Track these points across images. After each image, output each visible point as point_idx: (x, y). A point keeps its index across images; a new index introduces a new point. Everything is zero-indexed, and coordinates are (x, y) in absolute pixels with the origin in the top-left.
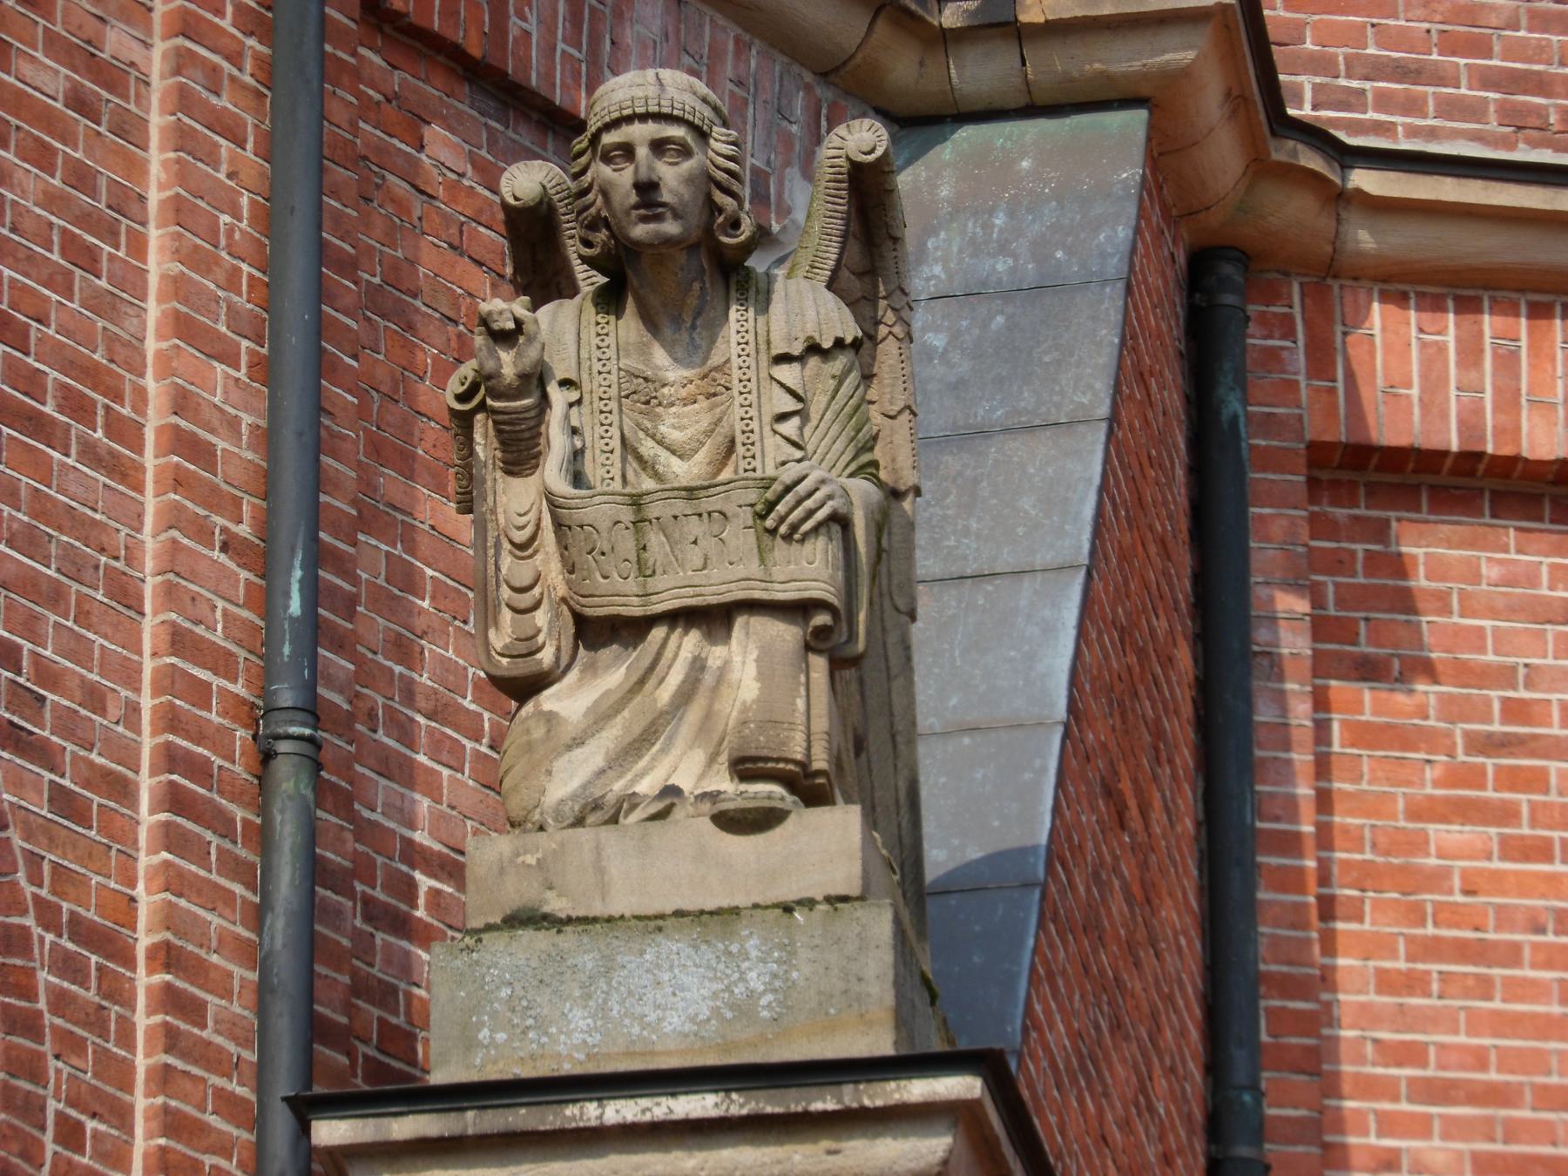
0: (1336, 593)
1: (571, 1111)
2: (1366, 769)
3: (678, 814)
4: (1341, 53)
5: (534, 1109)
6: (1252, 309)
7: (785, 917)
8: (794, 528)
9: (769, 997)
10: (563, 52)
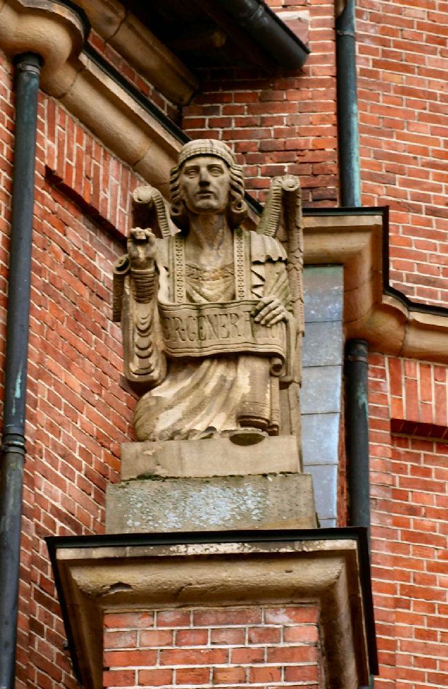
0: (400, 480)
1: (173, 548)
2: (411, 550)
3: (216, 437)
4: (404, 273)
5: (156, 547)
6: (371, 366)
7: (264, 480)
8: (267, 322)
9: (257, 511)
10: (120, 210)
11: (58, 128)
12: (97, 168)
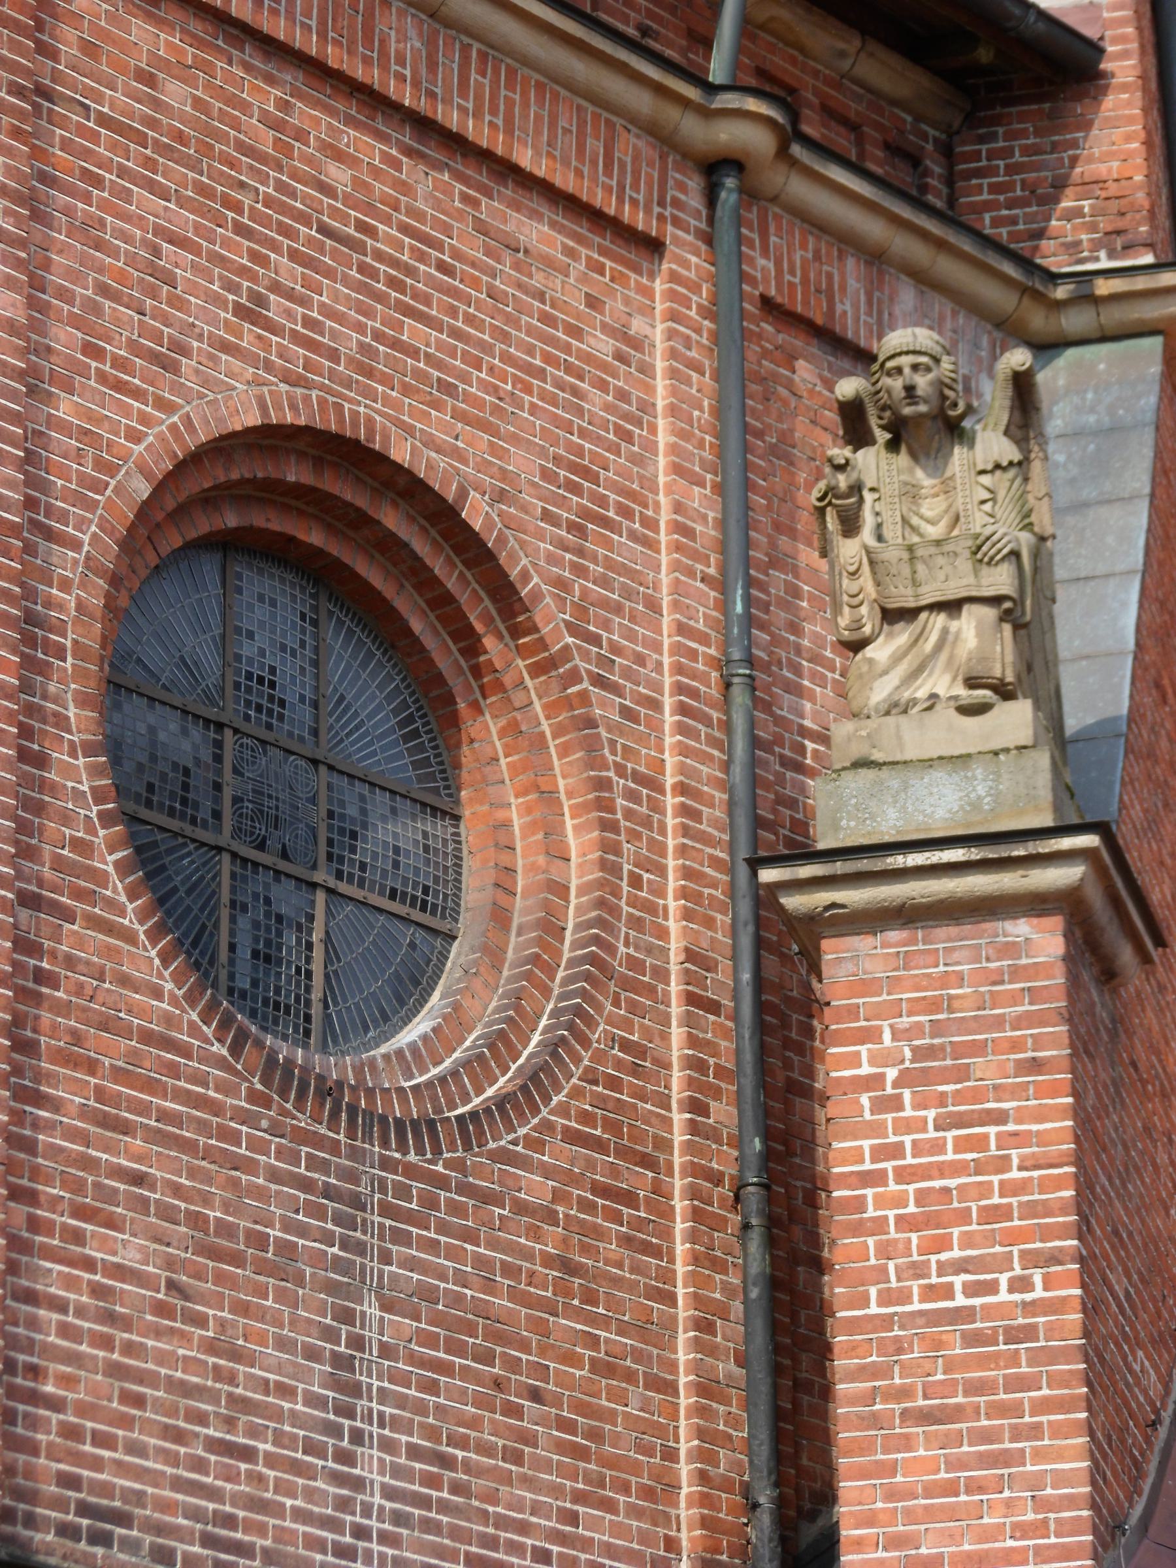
1: (890, 860)
3: (938, 707)
8: (992, 558)
11: (773, 239)
12: (830, 276)
